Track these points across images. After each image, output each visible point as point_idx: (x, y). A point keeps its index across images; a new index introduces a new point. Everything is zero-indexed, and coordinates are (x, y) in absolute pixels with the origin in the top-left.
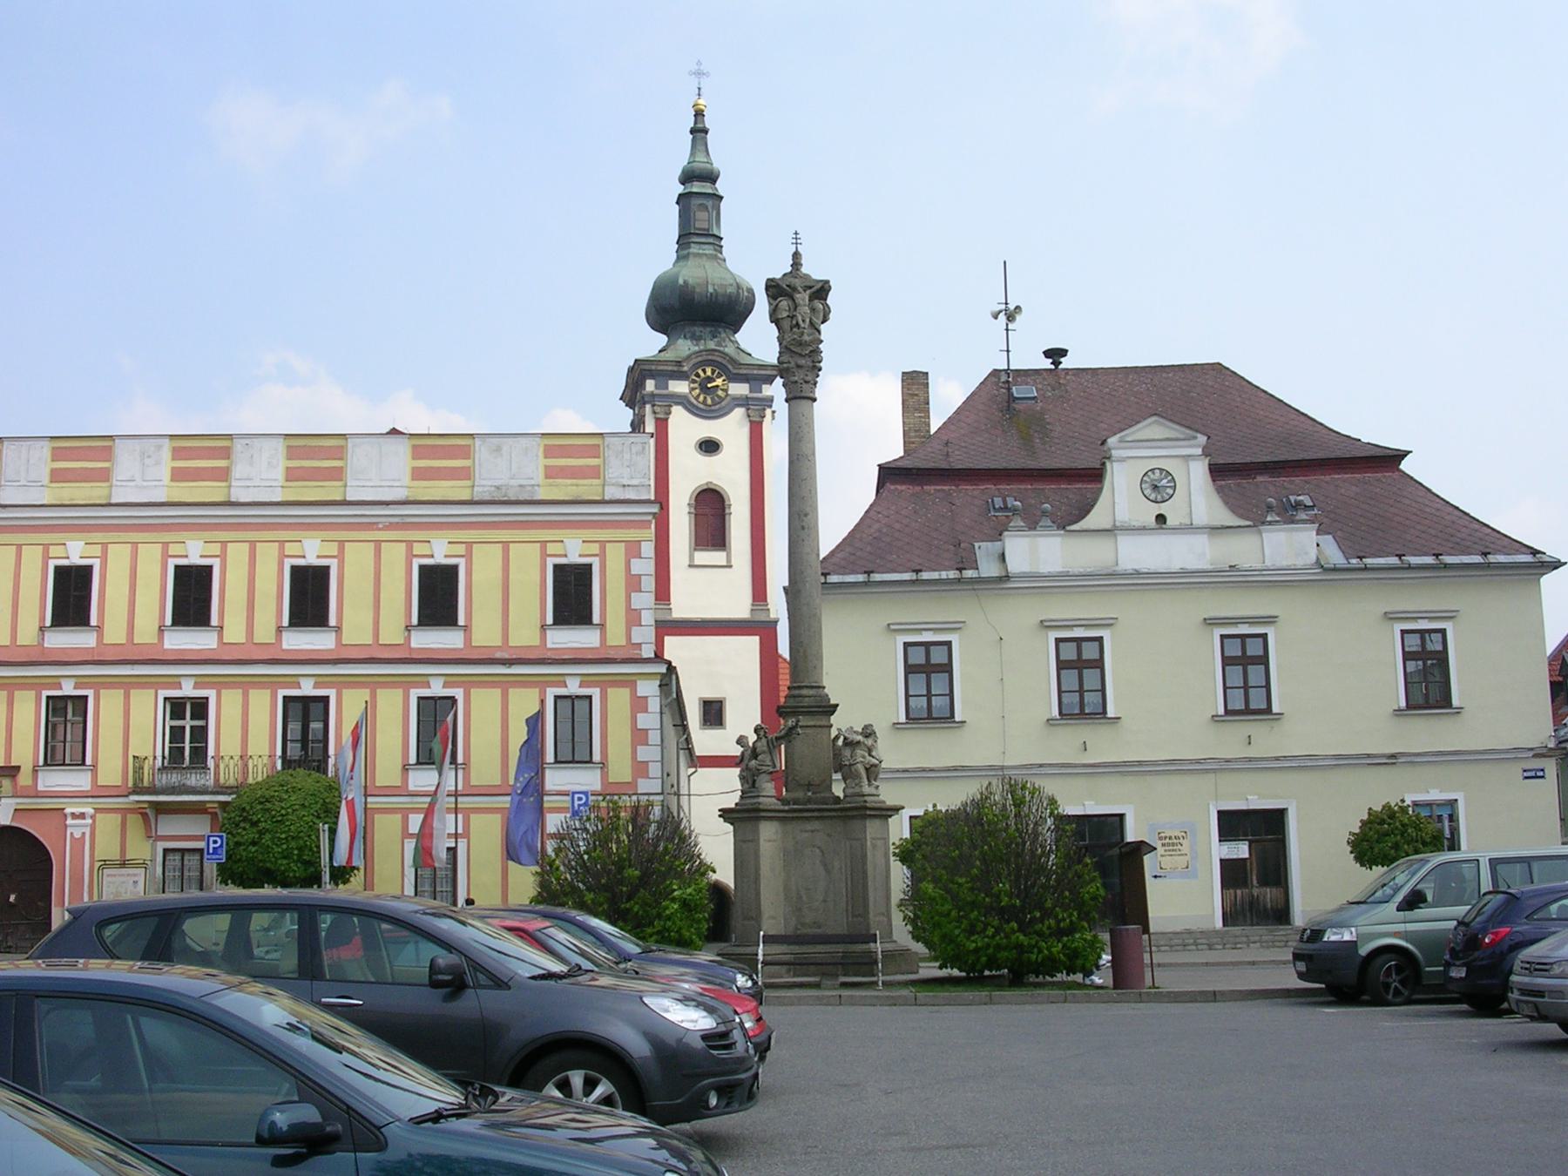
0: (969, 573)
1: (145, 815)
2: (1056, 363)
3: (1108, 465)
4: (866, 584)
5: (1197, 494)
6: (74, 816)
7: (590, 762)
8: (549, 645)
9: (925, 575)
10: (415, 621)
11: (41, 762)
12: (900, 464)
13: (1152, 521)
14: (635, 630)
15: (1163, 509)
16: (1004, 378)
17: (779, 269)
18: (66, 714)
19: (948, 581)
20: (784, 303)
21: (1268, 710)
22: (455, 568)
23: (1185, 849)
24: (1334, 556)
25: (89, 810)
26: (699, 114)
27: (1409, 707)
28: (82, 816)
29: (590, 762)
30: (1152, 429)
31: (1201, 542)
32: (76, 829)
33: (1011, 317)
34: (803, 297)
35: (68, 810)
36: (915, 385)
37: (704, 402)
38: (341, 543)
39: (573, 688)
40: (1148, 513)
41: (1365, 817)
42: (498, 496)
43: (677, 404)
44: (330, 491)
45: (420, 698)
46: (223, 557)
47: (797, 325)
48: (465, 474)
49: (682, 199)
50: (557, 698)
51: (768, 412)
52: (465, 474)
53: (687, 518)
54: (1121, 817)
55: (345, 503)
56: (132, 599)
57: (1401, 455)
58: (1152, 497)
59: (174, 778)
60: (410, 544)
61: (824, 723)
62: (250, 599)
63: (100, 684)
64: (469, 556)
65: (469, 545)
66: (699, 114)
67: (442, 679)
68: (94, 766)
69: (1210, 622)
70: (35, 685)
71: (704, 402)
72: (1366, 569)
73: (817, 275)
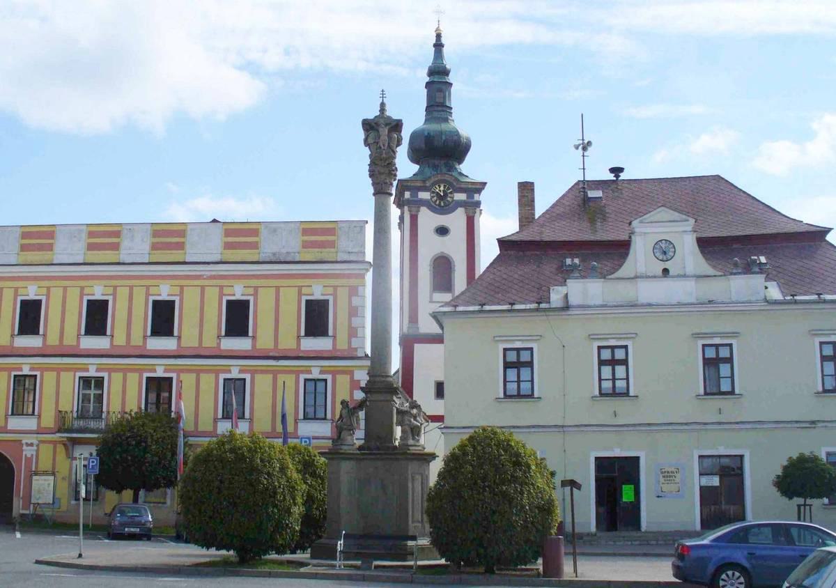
0: (543, 306)
1: (65, 445)
2: (617, 176)
3: (633, 237)
4: (509, 311)
5: (689, 256)
6: (28, 445)
7: (325, 419)
8: (302, 348)
9: (517, 307)
10: (223, 333)
11: (10, 413)
12: (513, 238)
13: (660, 273)
14: (353, 339)
15: (668, 265)
16: (581, 185)
17: (373, 113)
18: (23, 386)
19: (473, 312)
20: (372, 134)
21: (732, 393)
22: (248, 302)
23: (677, 480)
24: (774, 293)
25: (35, 442)
26: (439, 36)
27: (706, 394)
28: (32, 445)
29: (325, 419)
30: (663, 214)
31: (690, 285)
32: (28, 452)
33: (584, 149)
34: (384, 131)
35: (24, 442)
36: (526, 191)
37: (439, 205)
38: (115, 287)
39: (315, 374)
40: (658, 268)
41: (785, 463)
42: (274, 259)
43: (423, 205)
44: (109, 256)
45: (225, 380)
46: (114, 295)
47: (380, 147)
48: (255, 246)
49: (428, 85)
50: (306, 380)
51: (478, 210)
52: (255, 246)
53: (429, 272)
54: (637, 459)
55: (119, 264)
56: (65, 320)
57: (828, 230)
58: (661, 258)
59: (81, 423)
60: (221, 287)
61: (389, 398)
62: (130, 320)
63: (111, 370)
64: (255, 294)
65: (256, 288)
66: (439, 36)
67: (163, 367)
68: (39, 416)
69: (697, 336)
70: (216, 371)
71: (439, 205)
72: (796, 302)
73: (395, 117)
